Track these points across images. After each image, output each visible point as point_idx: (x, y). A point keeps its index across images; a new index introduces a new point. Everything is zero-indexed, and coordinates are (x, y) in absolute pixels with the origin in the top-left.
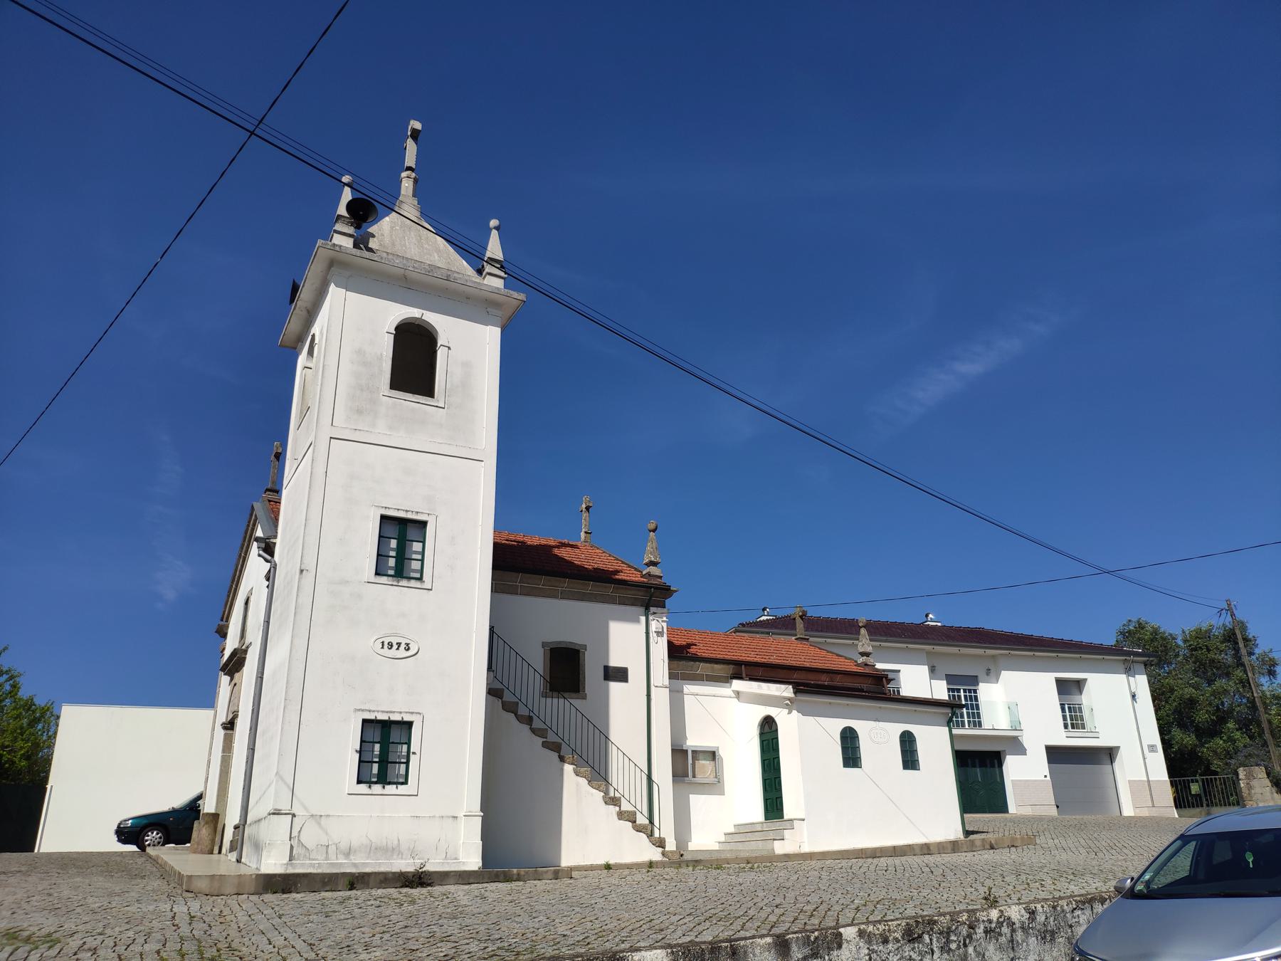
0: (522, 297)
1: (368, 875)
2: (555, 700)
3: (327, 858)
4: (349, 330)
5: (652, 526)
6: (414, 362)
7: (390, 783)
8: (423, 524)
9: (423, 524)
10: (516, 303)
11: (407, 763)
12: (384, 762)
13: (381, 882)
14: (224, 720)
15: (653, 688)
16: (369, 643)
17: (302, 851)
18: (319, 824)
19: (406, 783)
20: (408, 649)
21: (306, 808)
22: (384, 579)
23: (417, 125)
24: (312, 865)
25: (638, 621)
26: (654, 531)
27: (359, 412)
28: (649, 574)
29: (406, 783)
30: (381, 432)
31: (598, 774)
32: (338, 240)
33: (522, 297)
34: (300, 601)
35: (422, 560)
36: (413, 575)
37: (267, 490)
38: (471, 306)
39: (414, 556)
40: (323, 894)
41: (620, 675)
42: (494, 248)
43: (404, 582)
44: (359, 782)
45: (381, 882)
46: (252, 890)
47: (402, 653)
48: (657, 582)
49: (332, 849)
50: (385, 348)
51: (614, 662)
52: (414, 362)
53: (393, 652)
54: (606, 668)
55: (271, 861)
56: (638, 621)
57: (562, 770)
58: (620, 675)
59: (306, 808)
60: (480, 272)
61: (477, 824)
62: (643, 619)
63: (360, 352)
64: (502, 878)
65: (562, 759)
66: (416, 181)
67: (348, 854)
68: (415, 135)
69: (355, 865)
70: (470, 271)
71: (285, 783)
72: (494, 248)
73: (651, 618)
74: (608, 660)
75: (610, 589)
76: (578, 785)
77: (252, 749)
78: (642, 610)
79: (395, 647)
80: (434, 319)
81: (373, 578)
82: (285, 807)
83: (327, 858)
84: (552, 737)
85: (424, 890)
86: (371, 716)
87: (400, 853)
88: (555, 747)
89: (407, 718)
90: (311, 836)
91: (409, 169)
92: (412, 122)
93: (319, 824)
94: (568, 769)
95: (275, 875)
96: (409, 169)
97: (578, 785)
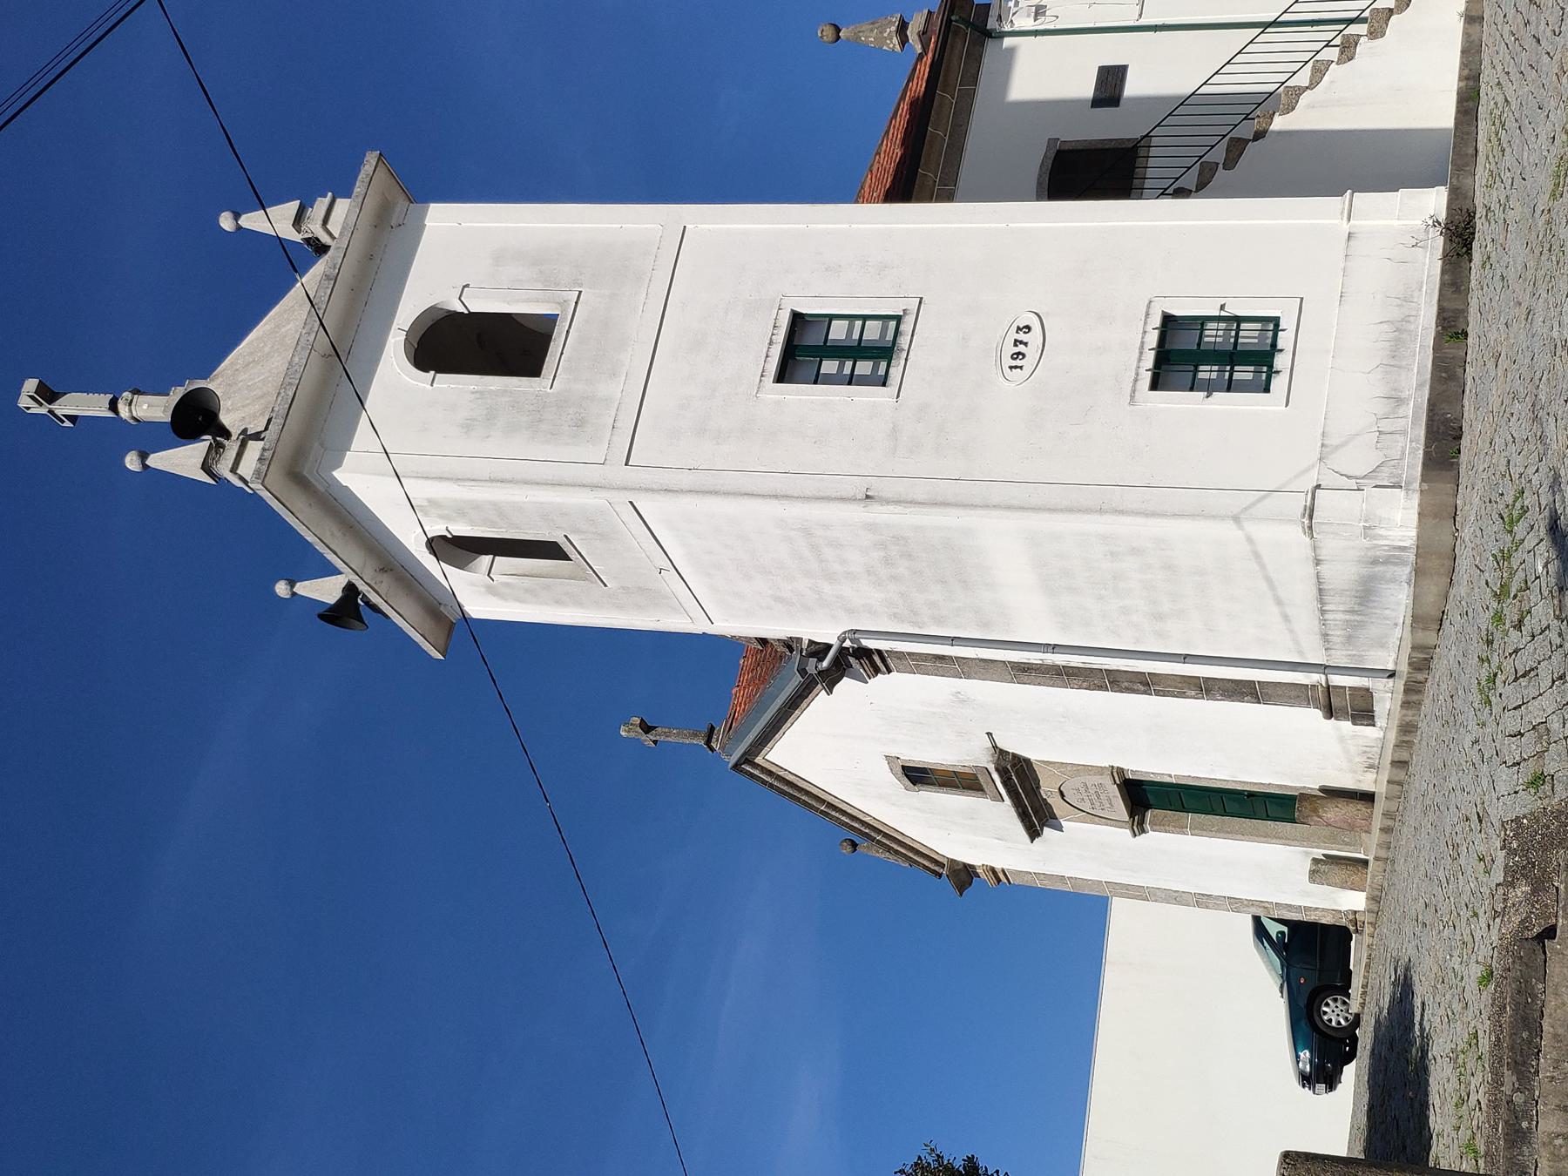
0: (371, 158)
1: (1441, 310)
2: (1150, 173)
3: (1404, 433)
4: (419, 462)
5: (829, 33)
6: (490, 346)
7: (1274, 345)
8: (797, 319)
9: (797, 319)
10: (382, 174)
11: (1239, 320)
12: (1232, 356)
13: (1458, 291)
14: (1128, 832)
15: (1143, 22)
16: (1011, 390)
17: (1386, 471)
18: (1337, 448)
19: (1276, 321)
20: (1028, 328)
21: (1307, 470)
22: (895, 373)
23: (31, 385)
24: (1413, 451)
25: (1012, 51)
26: (838, 30)
27: (580, 423)
28: (924, 35)
29: (1276, 321)
30: (622, 390)
31: (1288, 98)
32: (248, 467)
33: (371, 158)
34: (921, 497)
35: (865, 318)
36: (890, 337)
37: (708, 743)
38: (386, 249)
39: (856, 336)
40: (1466, 403)
41: (1111, 80)
42: (277, 221)
43: (904, 341)
44: (1267, 390)
45: (1458, 291)
46: (1449, 487)
47: (1034, 338)
48: (937, 22)
49: (1386, 425)
50: (461, 389)
51: (1087, 90)
52: (490, 346)
53: (1032, 352)
54: (1097, 102)
55: (1398, 516)
56: (1012, 51)
57: (1280, 133)
58: (1111, 80)
59: (1307, 470)
60: (322, 249)
61: (1363, 200)
62: (1008, 42)
63: (468, 427)
64: (1471, 104)
65: (1260, 135)
66: (136, 392)
67: (1400, 401)
68: (48, 394)
69: (1420, 386)
70: (320, 267)
71: (1254, 504)
72: (277, 221)
73: (1007, 28)
74: (1087, 100)
75: (946, 100)
76: (1311, 106)
77: (1185, 658)
78: (990, 45)
79: (1021, 348)
80: (408, 311)
81: (892, 389)
82: (1301, 502)
83: (1404, 433)
84: (1218, 155)
85: (1480, 223)
86: (1147, 378)
87: (1406, 319)
88: (1237, 148)
89: (1157, 321)
90: (1360, 459)
91: (113, 406)
92: (24, 402)
93: (1337, 448)
94: (1279, 123)
95: (1426, 453)
96: (113, 406)
97: (1311, 106)
